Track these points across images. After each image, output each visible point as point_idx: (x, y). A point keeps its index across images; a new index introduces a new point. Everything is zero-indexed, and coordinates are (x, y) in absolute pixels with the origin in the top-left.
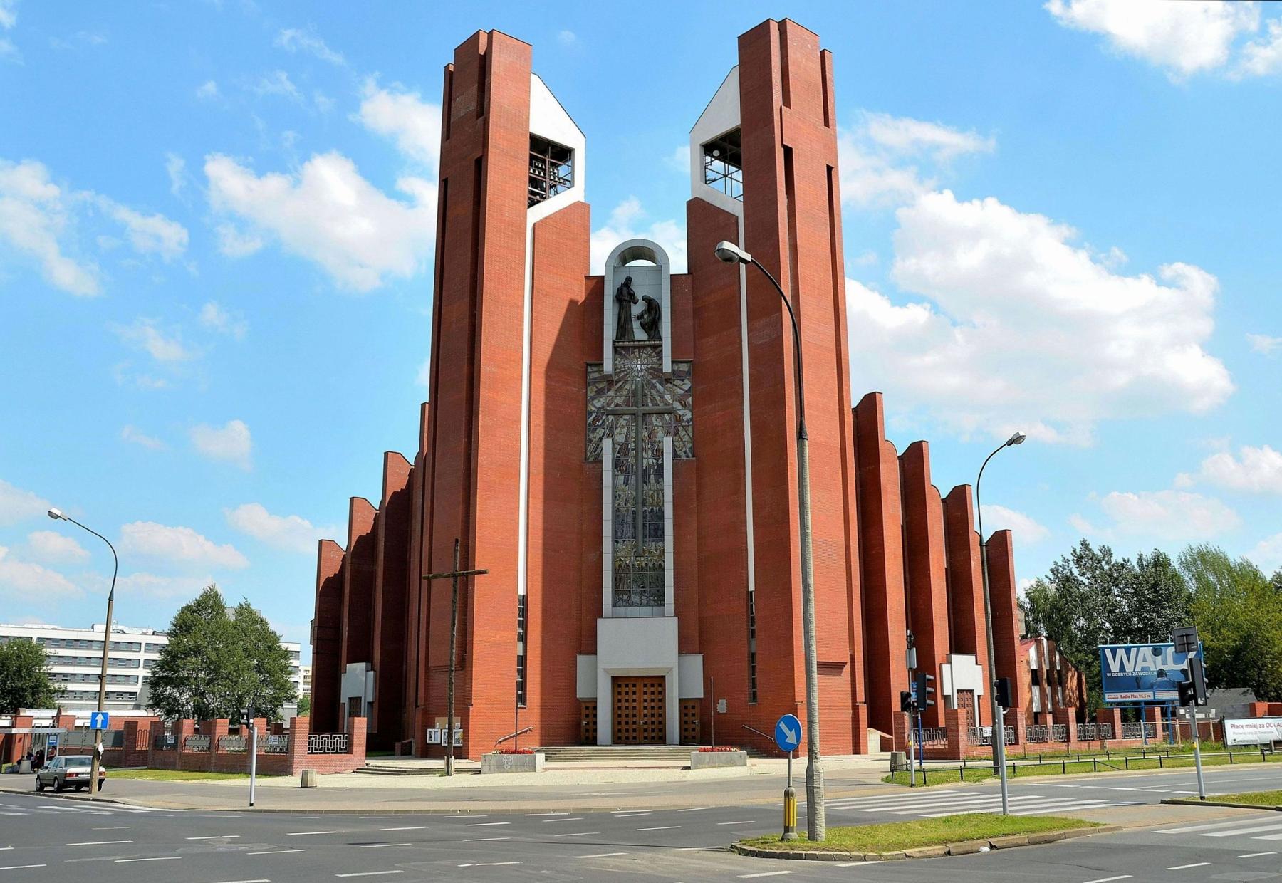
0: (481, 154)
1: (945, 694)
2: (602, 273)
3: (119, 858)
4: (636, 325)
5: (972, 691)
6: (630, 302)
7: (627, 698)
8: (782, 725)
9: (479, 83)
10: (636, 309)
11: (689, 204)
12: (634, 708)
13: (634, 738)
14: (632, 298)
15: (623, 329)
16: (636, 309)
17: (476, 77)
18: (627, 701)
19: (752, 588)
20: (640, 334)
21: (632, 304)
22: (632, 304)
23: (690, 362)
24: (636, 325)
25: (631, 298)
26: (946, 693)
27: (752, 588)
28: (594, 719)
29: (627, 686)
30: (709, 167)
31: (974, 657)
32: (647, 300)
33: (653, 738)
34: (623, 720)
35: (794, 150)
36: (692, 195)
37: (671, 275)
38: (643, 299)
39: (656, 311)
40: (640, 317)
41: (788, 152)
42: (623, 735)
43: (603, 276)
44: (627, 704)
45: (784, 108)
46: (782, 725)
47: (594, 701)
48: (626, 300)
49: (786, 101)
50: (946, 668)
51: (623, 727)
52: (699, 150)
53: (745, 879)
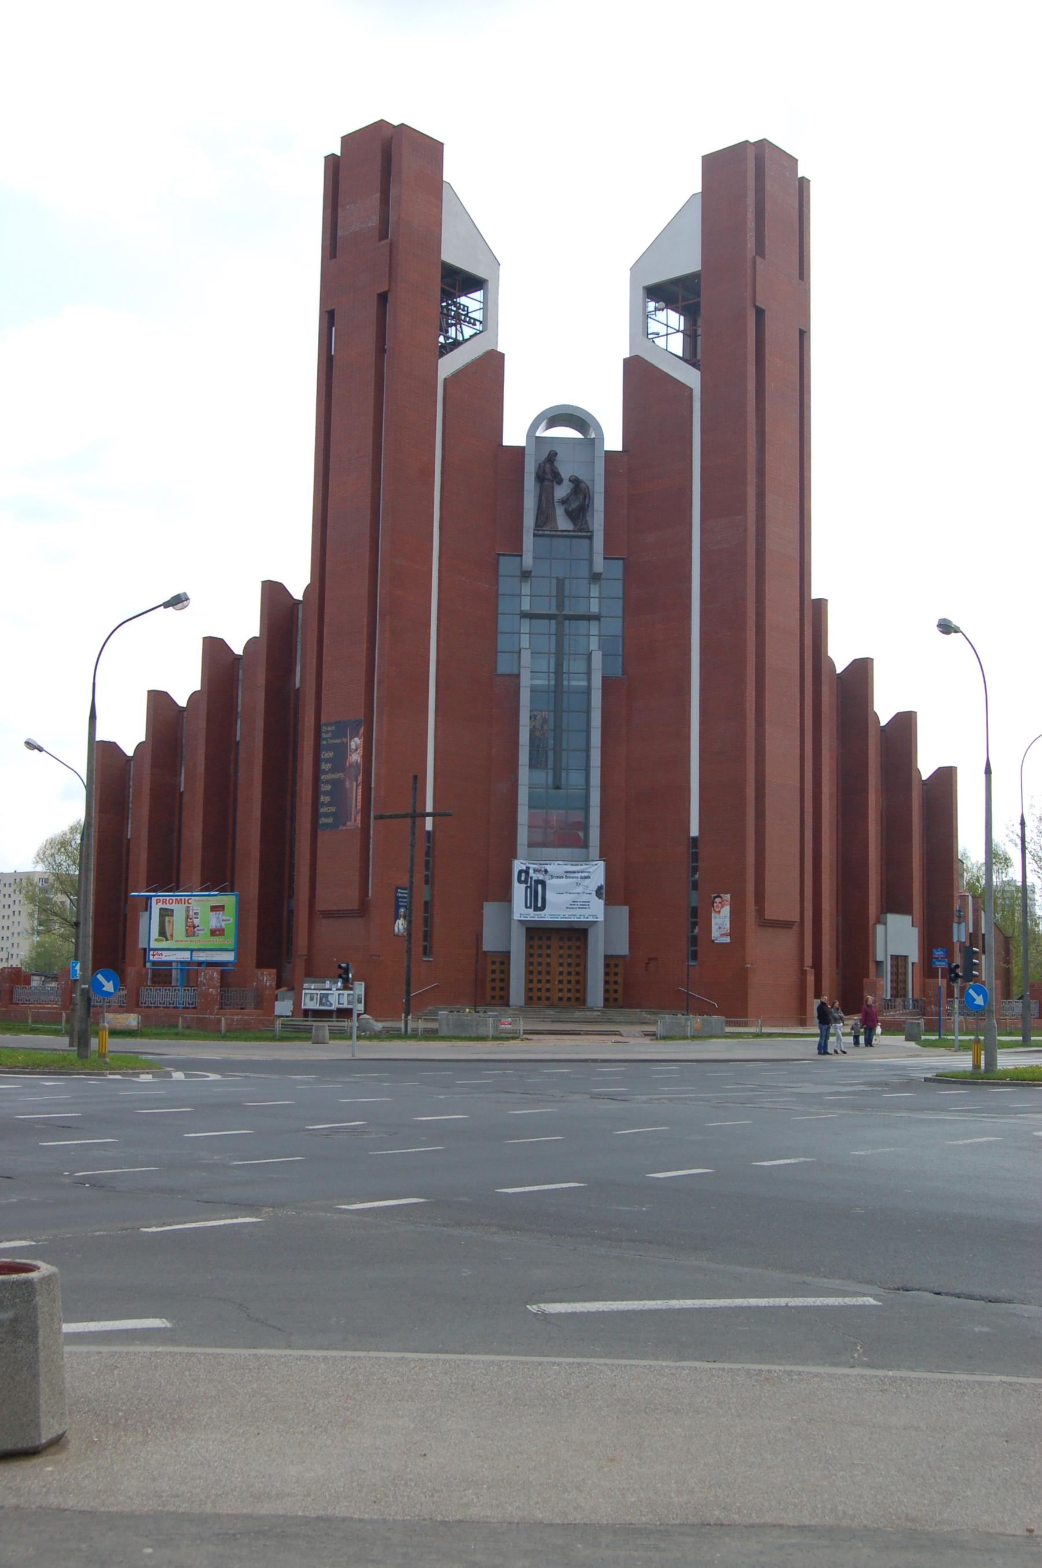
0: (387, 289)
1: (878, 960)
2: (522, 442)
3: (879, 1056)
4: (560, 511)
5: (906, 957)
6: (553, 482)
7: (540, 952)
8: (971, 991)
9: (381, 192)
10: (561, 492)
11: (627, 362)
12: (548, 964)
13: (548, 999)
14: (558, 479)
15: (544, 516)
16: (561, 492)
17: (378, 184)
18: (540, 956)
19: (694, 832)
20: (563, 523)
21: (555, 483)
22: (555, 483)
23: (623, 559)
24: (560, 511)
25: (555, 477)
26: (879, 959)
27: (694, 832)
28: (608, 978)
29: (540, 939)
30: (653, 317)
31: (911, 917)
32: (576, 482)
33: (569, 999)
34: (535, 977)
35: (766, 313)
36: (630, 352)
37: (606, 451)
38: (570, 481)
39: (585, 497)
40: (564, 502)
41: (760, 313)
42: (535, 994)
43: (524, 448)
44: (540, 960)
45: (759, 259)
46: (971, 991)
47: (507, 955)
48: (548, 480)
49: (760, 250)
50: (880, 928)
51: (535, 985)
52: (641, 292)
53: (251, 1217)
